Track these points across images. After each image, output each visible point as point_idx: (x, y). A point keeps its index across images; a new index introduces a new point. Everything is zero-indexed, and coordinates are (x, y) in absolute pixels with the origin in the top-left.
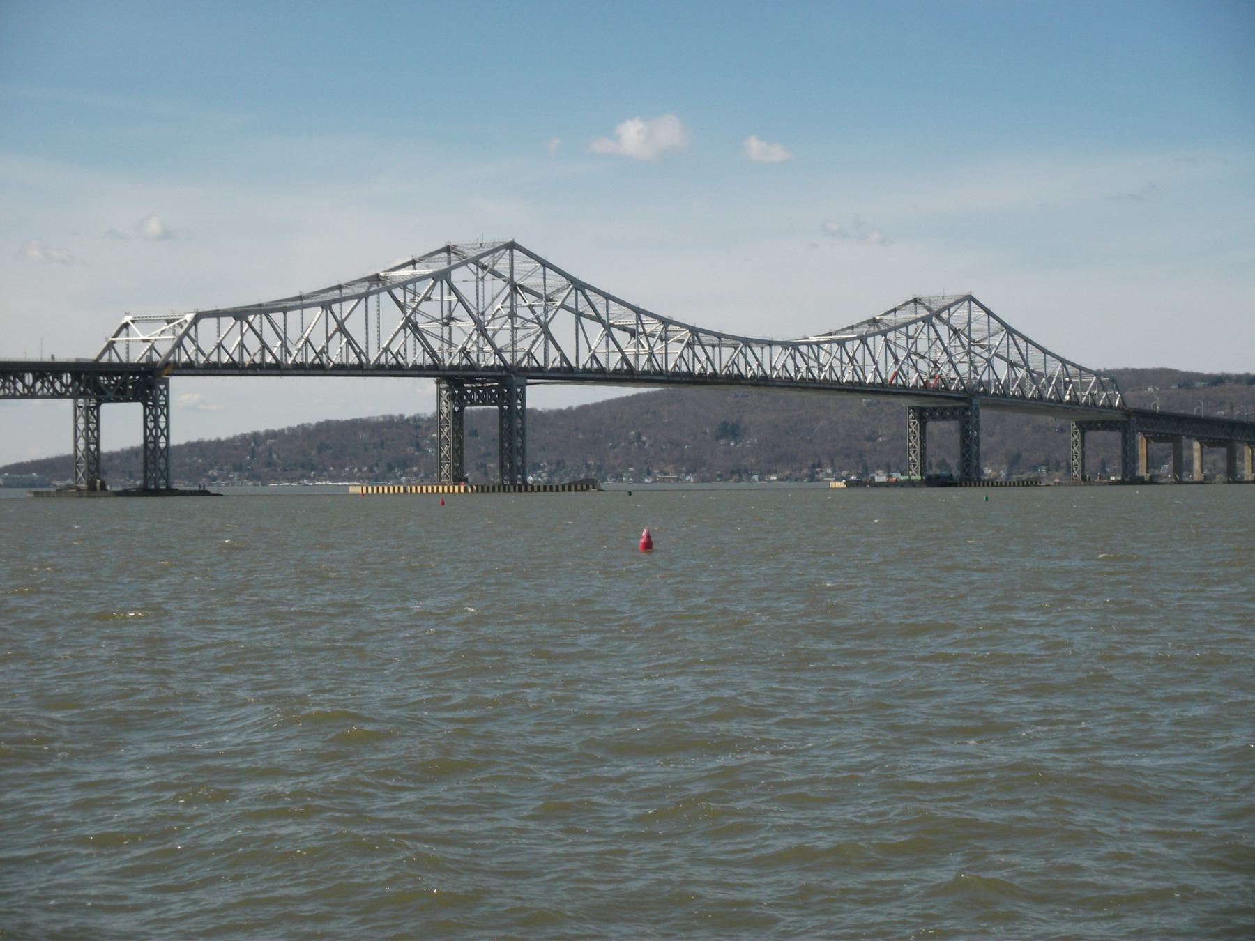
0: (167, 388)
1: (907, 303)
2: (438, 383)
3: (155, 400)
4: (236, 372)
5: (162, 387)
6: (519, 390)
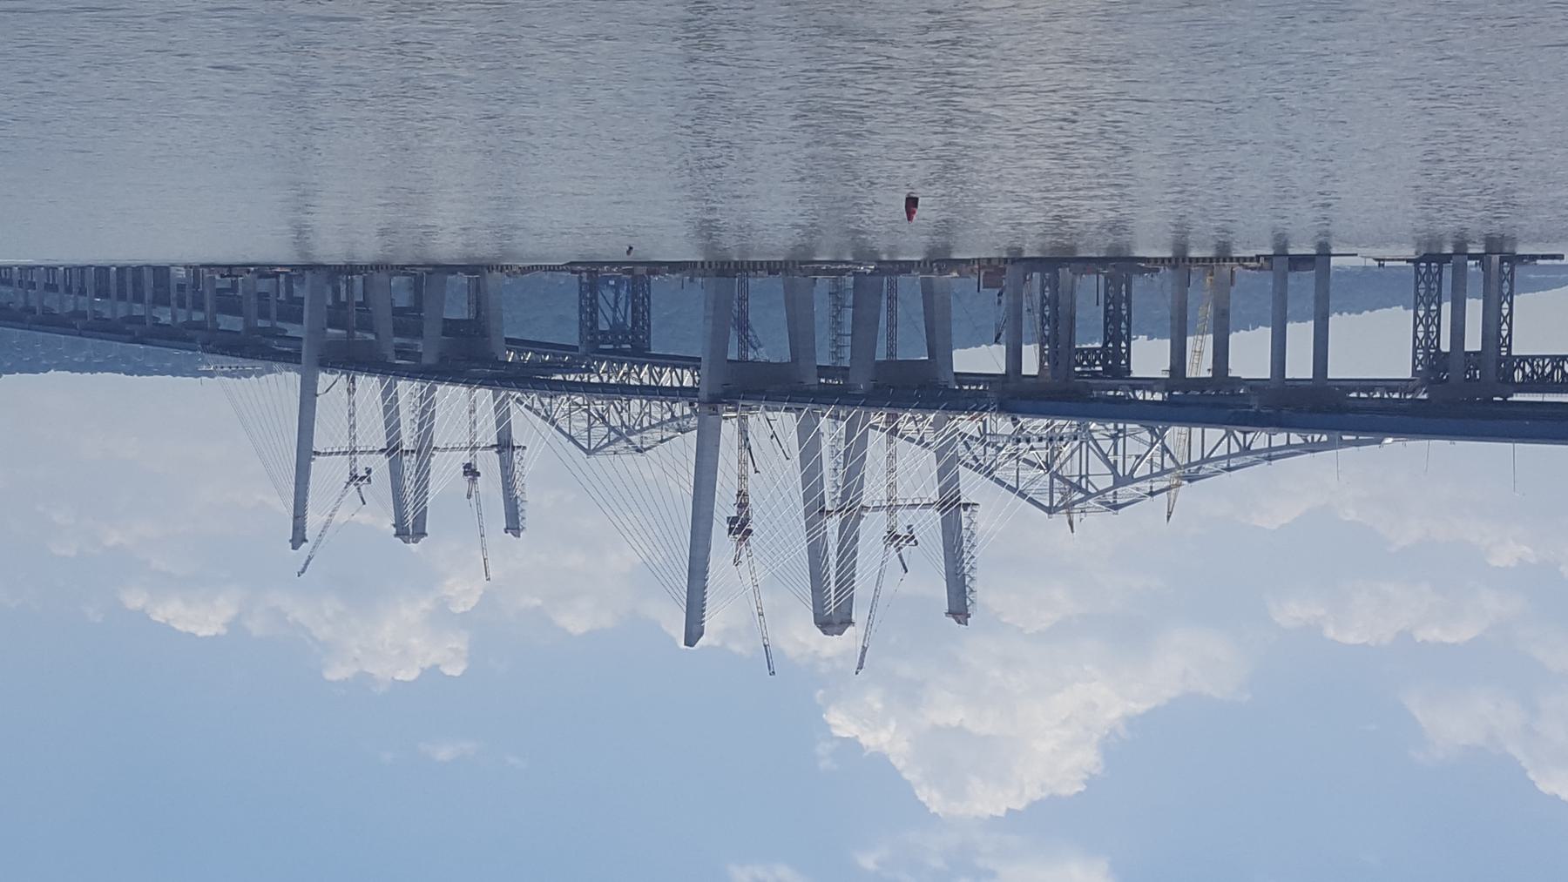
0: (1414, 367)
1: (649, 448)
2: (1129, 372)
3: (1426, 354)
4: (1388, 383)
5: (1419, 368)
6: (1046, 364)
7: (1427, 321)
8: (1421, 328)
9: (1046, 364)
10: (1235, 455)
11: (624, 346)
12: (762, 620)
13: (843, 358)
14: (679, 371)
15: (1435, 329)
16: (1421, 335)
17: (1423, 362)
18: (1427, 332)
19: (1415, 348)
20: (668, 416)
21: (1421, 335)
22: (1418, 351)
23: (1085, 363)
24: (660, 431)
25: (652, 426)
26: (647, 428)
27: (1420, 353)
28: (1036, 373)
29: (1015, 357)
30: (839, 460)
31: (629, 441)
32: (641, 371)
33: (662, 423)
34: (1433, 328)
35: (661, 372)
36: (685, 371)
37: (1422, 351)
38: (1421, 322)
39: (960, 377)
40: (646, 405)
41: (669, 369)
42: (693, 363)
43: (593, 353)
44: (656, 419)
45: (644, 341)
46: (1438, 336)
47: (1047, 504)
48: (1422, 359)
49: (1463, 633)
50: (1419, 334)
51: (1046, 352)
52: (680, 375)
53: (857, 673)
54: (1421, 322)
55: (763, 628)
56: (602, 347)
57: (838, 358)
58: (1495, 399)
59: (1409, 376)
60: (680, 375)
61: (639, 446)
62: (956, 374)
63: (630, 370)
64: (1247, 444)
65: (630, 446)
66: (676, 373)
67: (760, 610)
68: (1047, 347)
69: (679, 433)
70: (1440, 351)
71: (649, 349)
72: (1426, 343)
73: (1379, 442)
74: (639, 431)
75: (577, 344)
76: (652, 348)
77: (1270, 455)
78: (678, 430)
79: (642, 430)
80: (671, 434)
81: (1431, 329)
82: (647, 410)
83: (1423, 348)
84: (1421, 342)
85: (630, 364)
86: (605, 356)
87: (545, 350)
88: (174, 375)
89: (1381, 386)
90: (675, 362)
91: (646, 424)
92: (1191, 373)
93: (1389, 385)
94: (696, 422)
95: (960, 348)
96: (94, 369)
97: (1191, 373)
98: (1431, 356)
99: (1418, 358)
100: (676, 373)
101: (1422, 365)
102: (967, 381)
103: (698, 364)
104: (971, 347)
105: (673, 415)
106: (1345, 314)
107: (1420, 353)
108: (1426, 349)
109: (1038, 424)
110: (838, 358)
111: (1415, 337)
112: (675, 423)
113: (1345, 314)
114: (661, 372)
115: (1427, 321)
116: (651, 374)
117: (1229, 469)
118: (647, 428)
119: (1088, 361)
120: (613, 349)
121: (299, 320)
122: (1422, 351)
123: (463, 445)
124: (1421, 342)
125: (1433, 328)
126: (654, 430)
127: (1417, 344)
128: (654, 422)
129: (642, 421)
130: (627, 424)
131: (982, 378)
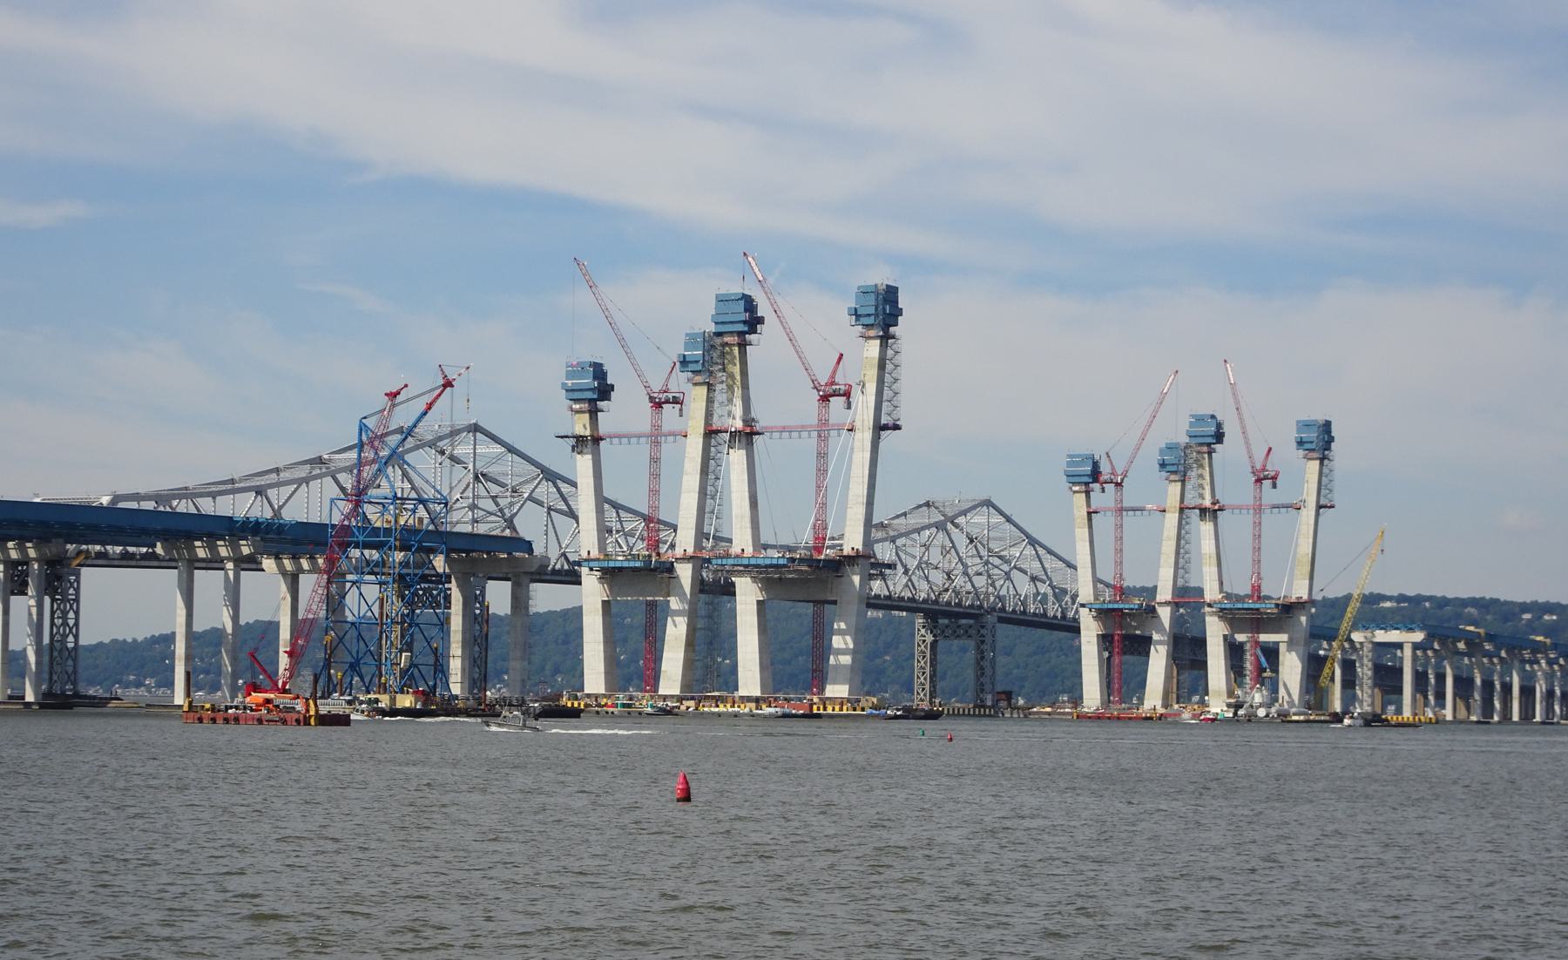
3: (65, 594)
4: (155, 563)
7: (64, 630)
8: (71, 622)
9: (478, 592)
10: (271, 486)
11: (946, 621)
13: (706, 603)
15: (56, 620)
16: (71, 615)
17: (69, 585)
18: (64, 616)
19: (77, 600)
21: (71, 615)
22: (74, 597)
23: (435, 592)
27: (72, 595)
28: (490, 583)
29: (520, 601)
30: (712, 488)
34: (58, 622)
37: (70, 597)
38: (71, 630)
42: (919, 605)
43: (982, 615)
46: (53, 613)
47: (478, 434)
48: (70, 588)
50: (74, 617)
51: (478, 605)
54: (71, 630)
56: (972, 621)
57: (712, 603)
58: (1406, 604)
59: (84, 570)
68: (478, 612)
70: (50, 597)
72: (65, 607)
73: (117, 498)
75: (999, 625)
77: (230, 487)
80: (895, 522)
81: (60, 620)
83: (69, 601)
84: (71, 607)
86: (969, 611)
87: (1036, 619)
88: (1444, 598)
89: (114, 559)
90: (889, 603)
92: (507, 586)
93: (103, 560)
95: (556, 611)
96: (1512, 602)
97: (507, 586)
98: (59, 591)
99: (75, 590)
101: (70, 582)
102: (566, 575)
104: (545, 613)
106: (130, 640)
107: (72, 595)
108: (65, 600)
109: (1294, 586)
110: (712, 603)
111: (77, 613)
113: (130, 640)
115: (64, 630)
117: (277, 470)
119: (431, 595)
121: (887, 692)
122: (70, 597)
123: (671, 439)
124: (71, 607)
125: (58, 622)
127: (75, 605)
131: (549, 578)
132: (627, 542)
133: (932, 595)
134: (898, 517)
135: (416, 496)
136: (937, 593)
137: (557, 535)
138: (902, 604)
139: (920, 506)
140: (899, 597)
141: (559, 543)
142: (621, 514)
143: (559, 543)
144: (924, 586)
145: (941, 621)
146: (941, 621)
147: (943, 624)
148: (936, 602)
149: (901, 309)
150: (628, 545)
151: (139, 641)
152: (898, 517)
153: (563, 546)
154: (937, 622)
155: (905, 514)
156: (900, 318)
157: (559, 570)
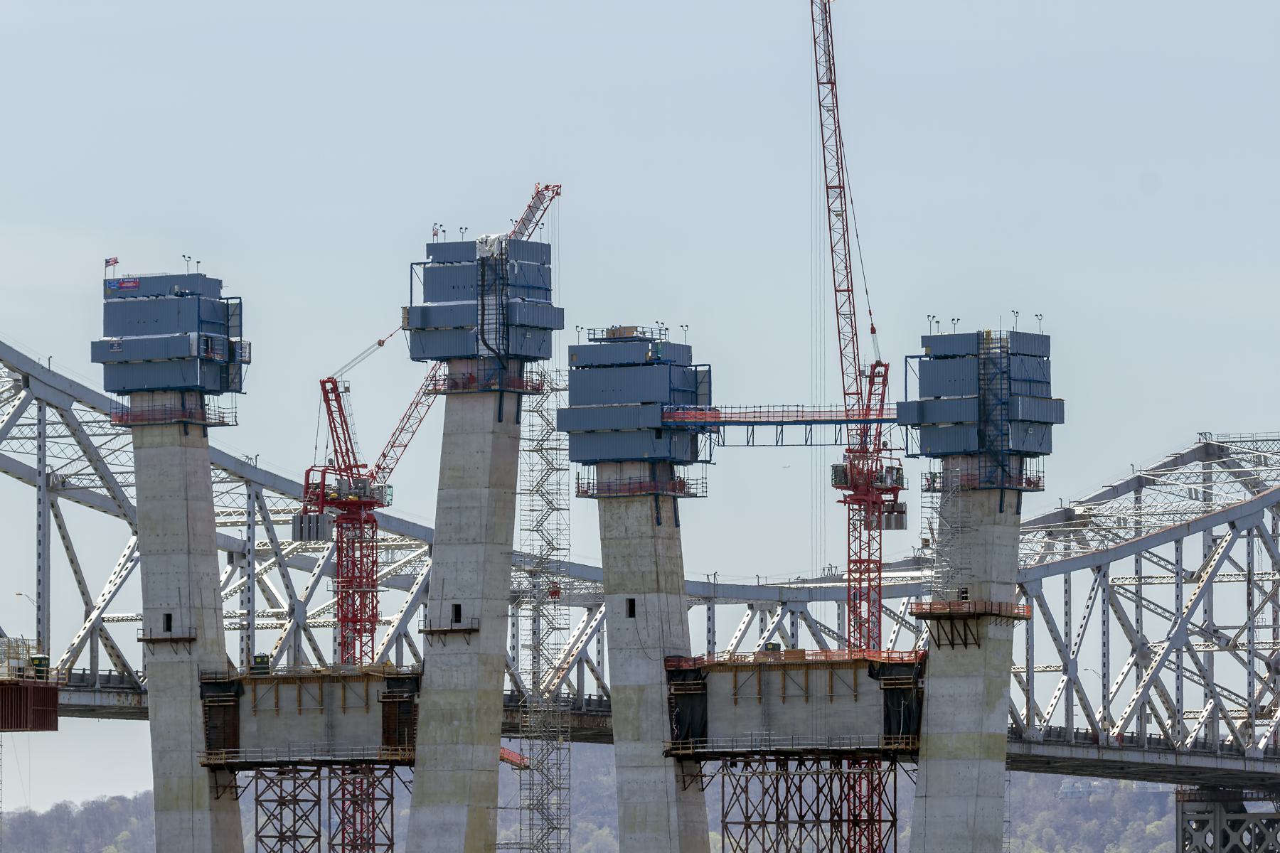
12: (831, 174)
14: (1081, 723)
20: (1121, 570)
24: (1147, 521)
25: (1176, 535)
26: (1189, 528)
31: (1254, 484)
32: (1211, 723)
33: (1140, 547)
35: (1143, 720)
36: (1058, 721)
39: (131, 701)
40: (1192, 610)
41: (1115, 731)
44: (1160, 561)
45: (1202, 824)
49: (1044, 830)
52: (1078, 709)
53: (789, 467)
55: (840, 247)
60: (1078, 709)
61: (1216, 468)
62: (141, 713)
63: (1248, 725)
64: (816, 764)
65: (1248, 467)
66: (1089, 716)
67: (836, 205)
69: (1079, 510)
71: (1181, 798)
74: (1216, 519)
76: (1172, 798)
78: (1084, 521)
79: (1204, 524)
80: (1104, 509)
82: (1190, 591)
85: (1248, 747)
90: (1092, 754)
91: (1194, 546)
94: (1023, 550)
100: (1089, 716)
103: (1016, 749)
105: (1101, 571)
112: (1094, 545)
114: (1143, 720)
116: (1176, 713)
118: (1189, 528)
120: (373, 764)
126: (1167, 522)
128: (1166, 550)
129: (1207, 557)
130: (1257, 542)
132: (288, 586)
133: (1223, 729)
134: (1115, 492)
135: (301, 595)
136: (1238, 723)
137: (77, 571)
138: (1132, 757)
139: (1179, 460)
140: (1120, 736)
141: (84, 593)
142: (269, 505)
143: (84, 593)
144: (1194, 699)
145: (1253, 808)
146: (1253, 808)
147: (1259, 816)
148: (1236, 751)
149: (1060, 402)
150: (292, 596)
151: (38, 815)
152: (1115, 492)
153: (99, 602)
154: (1243, 810)
155: (1138, 484)
156: (1055, 428)
157: (1131, 739)
